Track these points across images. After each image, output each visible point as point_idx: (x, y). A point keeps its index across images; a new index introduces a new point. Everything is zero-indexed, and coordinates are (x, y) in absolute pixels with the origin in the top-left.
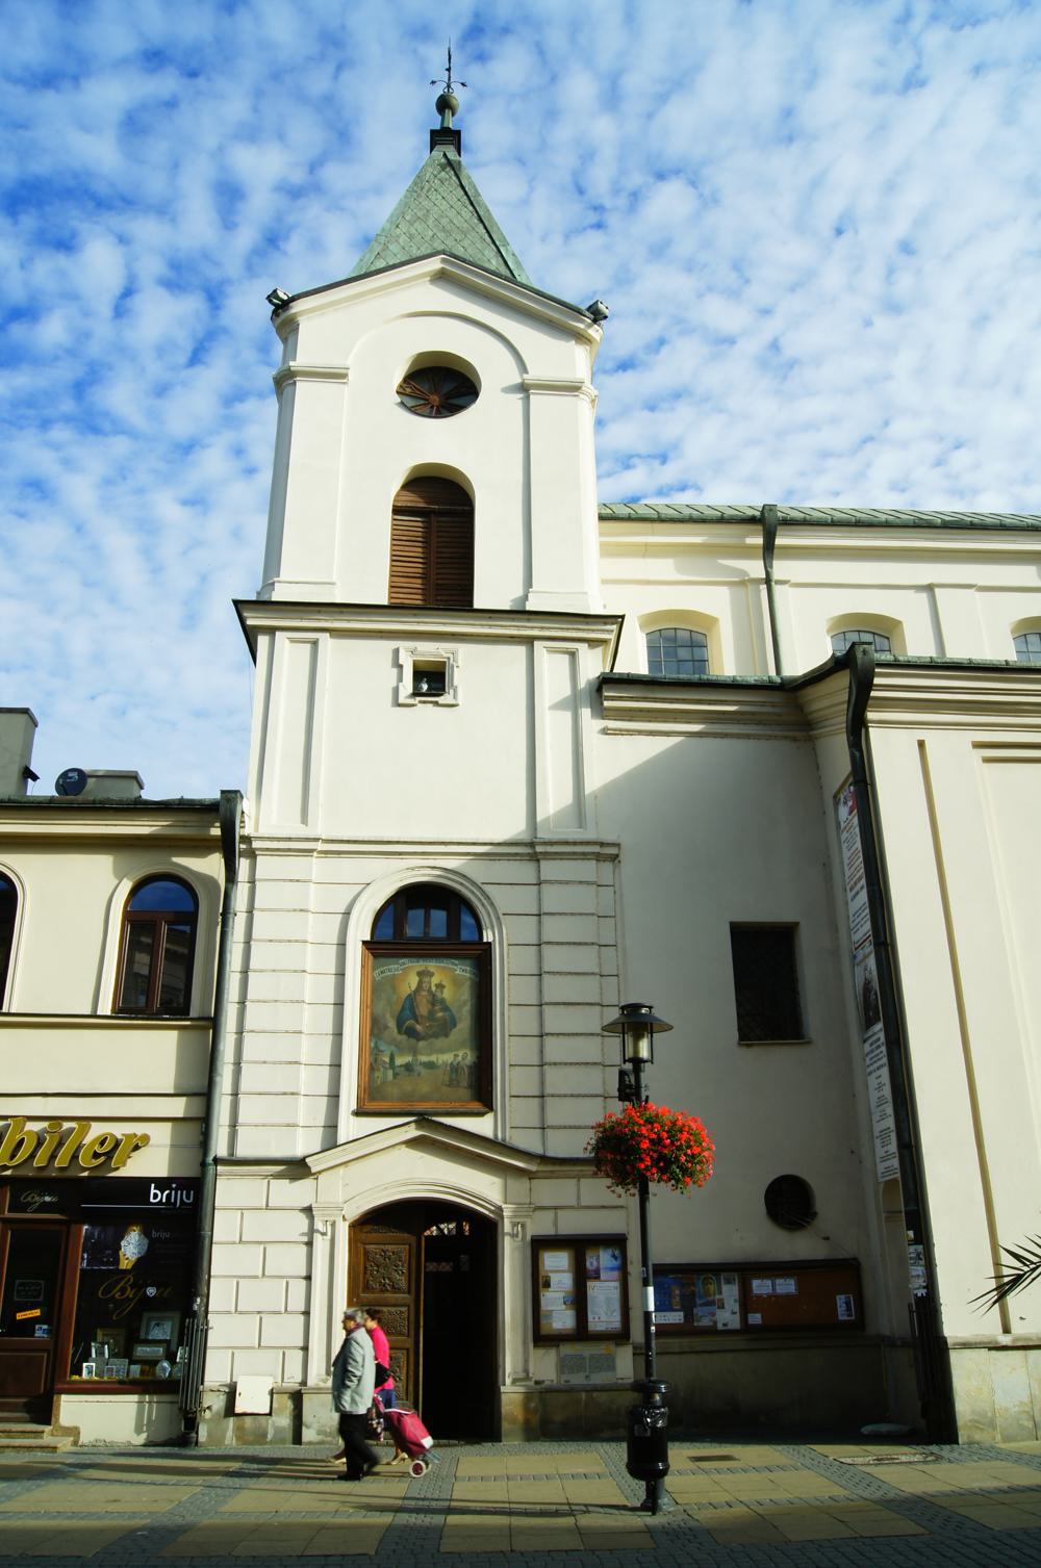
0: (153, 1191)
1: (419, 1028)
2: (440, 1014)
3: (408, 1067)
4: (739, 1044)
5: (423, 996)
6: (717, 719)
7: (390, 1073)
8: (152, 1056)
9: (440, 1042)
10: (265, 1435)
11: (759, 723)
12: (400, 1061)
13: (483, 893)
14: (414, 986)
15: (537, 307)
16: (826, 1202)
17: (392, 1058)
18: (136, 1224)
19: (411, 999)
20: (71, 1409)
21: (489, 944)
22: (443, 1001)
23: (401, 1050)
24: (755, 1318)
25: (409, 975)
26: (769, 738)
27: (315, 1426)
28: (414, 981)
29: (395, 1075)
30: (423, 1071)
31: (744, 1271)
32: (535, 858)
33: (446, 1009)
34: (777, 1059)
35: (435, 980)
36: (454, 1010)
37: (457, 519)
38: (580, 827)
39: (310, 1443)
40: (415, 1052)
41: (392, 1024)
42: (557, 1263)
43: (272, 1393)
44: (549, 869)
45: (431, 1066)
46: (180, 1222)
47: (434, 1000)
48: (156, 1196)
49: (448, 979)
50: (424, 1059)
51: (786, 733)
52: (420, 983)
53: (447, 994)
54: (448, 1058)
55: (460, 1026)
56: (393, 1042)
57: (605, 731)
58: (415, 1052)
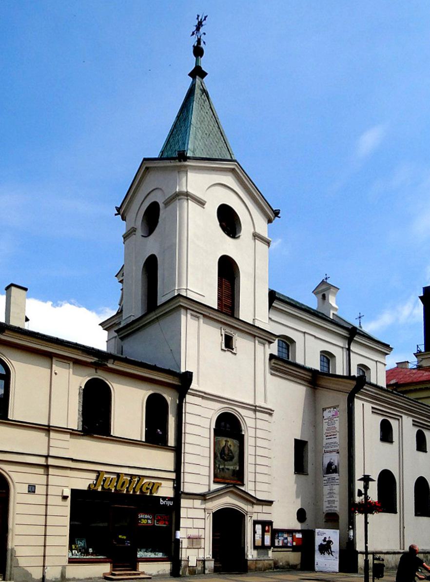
0: (161, 501)
1: (225, 457)
2: (230, 454)
3: (223, 469)
4: (295, 473)
5: (226, 449)
6: (228, 297)
7: (219, 470)
8: (163, 460)
9: (230, 463)
10: (195, 572)
11: (305, 381)
12: (221, 467)
13: (243, 419)
14: (224, 444)
15: (269, 213)
16: (309, 516)
17: (219, 466)
18: (356, 504)
19: (224, 448)
20: (142, 567)
21: (243, 435)
22: (231, 450)
23: (222, 464)
24: (294, 544)
25: (223, 441)
26: (308, 386)
27: (208, 569)
28: (224, 443)
29: (220, 471)
30: (227, 471)
31: (290, 532)
32: (255, 411)
33: (232, 453)
34: (302, 477)
35: (229, 443)
36: (234, 453)
37: (306, 373)
38: (265, 403)
39: (207, 574)
40: (225, 465)
41: (219, 455)
42: (259, 528)
43: (197, 560)
44: (259, 415)
45: (228, 469)
46: (171, 513)
47: (229, 450)
48: (162, 502)
49: (232, 443)
50: (226, 467)
51: (309, 385)
52: (226, 444)
53: (232, 448)
54: (231, 468)
55: (235, 458)
56: (219, 461)
57: (272, 374)
58: (225, 465)
